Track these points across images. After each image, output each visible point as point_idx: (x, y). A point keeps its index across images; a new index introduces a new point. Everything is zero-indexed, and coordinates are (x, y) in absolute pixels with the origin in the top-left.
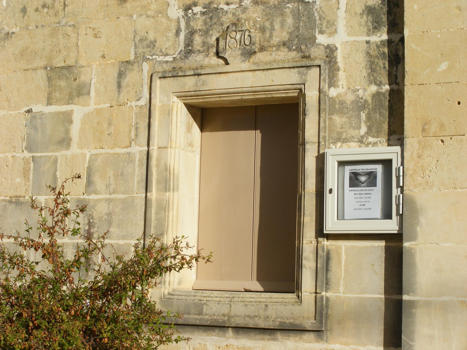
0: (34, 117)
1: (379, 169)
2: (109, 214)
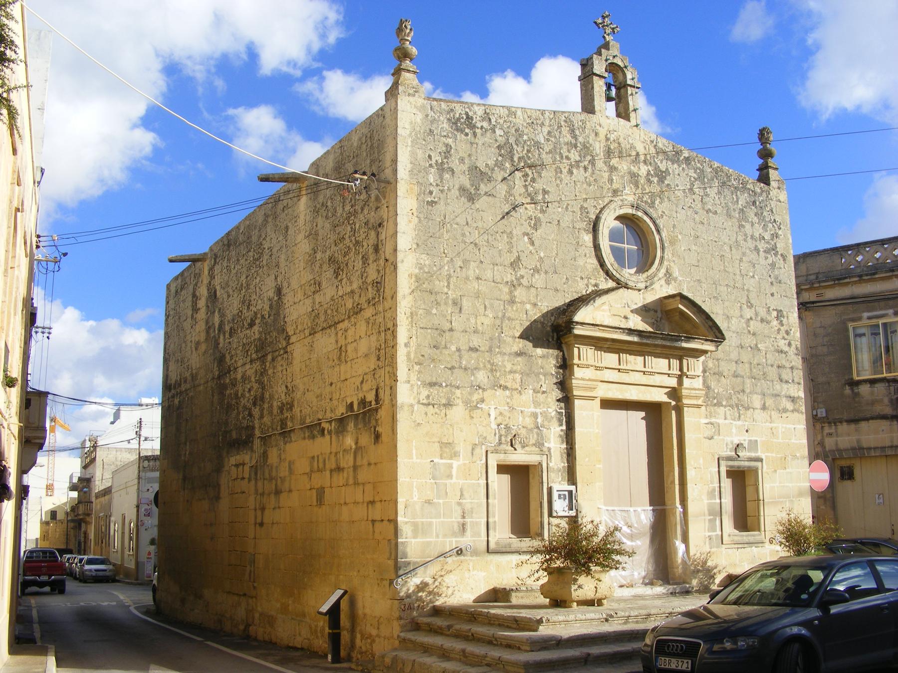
0: (435, 464)
1: (566, 493)
2: (472, 508)
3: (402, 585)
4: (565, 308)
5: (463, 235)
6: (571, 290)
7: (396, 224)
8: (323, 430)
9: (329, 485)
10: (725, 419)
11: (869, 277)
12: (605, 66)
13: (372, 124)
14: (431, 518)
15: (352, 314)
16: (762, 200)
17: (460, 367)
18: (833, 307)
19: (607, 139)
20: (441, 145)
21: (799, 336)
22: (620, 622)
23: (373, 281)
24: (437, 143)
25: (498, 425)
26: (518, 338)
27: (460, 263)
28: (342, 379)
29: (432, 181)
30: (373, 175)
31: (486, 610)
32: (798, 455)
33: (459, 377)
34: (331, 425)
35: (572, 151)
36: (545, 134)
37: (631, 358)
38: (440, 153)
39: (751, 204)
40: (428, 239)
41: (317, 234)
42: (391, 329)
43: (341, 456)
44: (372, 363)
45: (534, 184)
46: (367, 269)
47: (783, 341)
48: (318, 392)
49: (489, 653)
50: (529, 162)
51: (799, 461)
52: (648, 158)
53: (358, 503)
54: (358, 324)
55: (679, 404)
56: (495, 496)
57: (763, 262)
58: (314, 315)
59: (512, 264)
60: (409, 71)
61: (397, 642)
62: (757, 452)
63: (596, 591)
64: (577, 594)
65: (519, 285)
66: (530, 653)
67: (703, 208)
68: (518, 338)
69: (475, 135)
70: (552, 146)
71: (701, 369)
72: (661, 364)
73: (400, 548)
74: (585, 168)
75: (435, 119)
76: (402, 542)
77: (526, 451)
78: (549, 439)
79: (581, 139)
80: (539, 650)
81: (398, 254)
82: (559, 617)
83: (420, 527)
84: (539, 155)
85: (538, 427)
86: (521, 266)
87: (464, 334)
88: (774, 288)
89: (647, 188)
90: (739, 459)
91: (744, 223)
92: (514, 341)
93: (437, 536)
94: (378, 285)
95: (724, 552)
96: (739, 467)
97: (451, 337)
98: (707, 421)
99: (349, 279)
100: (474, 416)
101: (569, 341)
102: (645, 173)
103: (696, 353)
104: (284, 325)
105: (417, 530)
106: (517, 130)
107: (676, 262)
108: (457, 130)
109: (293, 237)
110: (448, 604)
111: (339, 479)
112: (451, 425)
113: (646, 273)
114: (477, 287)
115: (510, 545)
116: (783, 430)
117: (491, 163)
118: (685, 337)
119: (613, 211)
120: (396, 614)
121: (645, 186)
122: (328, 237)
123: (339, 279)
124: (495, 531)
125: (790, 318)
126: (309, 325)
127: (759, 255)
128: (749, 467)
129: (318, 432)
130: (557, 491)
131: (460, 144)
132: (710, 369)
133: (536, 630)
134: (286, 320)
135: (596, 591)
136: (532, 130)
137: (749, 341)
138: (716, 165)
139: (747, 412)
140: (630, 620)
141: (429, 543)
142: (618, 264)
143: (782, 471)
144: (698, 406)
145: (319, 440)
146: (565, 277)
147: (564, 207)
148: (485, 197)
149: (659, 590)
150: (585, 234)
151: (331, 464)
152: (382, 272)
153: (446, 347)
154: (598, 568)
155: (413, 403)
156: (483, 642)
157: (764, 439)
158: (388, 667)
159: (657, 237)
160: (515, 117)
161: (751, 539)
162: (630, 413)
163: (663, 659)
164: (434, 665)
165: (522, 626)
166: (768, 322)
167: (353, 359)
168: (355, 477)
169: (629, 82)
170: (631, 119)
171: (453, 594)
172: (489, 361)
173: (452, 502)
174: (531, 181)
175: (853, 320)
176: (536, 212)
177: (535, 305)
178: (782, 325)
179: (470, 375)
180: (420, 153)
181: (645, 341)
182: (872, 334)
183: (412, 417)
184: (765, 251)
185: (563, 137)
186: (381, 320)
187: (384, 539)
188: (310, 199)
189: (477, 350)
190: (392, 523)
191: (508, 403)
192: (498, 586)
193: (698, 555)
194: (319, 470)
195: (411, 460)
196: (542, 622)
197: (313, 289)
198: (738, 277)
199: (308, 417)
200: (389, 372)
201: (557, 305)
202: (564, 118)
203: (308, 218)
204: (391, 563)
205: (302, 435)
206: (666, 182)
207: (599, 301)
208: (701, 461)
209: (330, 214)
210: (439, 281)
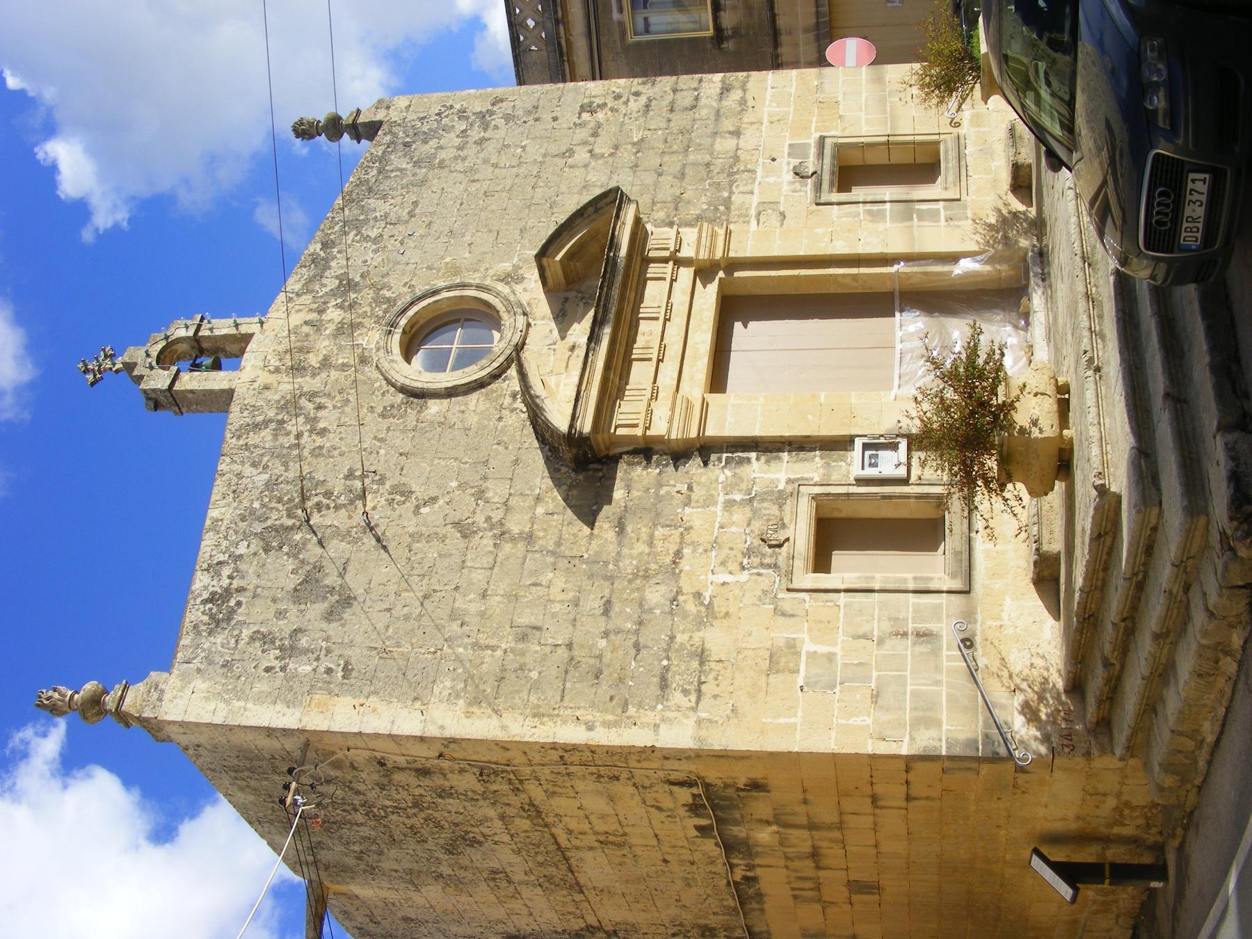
0: (807, 684)
1: (867, 453)
2: (890, 619)
3: (1026, 749)
4: (547, 447)
5: (407, 618)
6: (518, 438)
7: (377, 736)
8: (745, 878)
9: (844, 873)
10: (752, 193)
11: (559, 9)
12: (161, 371)
13: (213, 767)
14: (905, 693)
15: (540, 821)
16: (404, 132)
17: (637, 632)
18: (603, 65)
19: (277, 370)
20: (250, 650)
21: (624, 80)
22: (1100, 346)
23: (479, 781)
24: (246, 656)
25: (743, 568)
26: (592, 529)
27: (455, 626)
28: (655, 842)
29: (309, 668)
30: (290, 771)
31: (1077, 595)
32: (816, 83)
33: (654, 636)
34: (737, 865)
35: (289, 428)
36: (255, 471)
37: (640, 341)
38: (263, 652)
39: (407, 149)
40: (408, 681)
41: (410, 872)
42: (561, 753)
43: (791, 850)
44: (624, 789)
45: (335, 494)
46: (461, 790)
47: (632, 104)
48: (679, 884)
49: (1164, 585)
50: (297, 500)
51: (825, 81)
52: (315, 306)
53: (875, 824)
54: (561, 812)
55: (722, 265)
56: (868, 577)
57: (501, 132)
58: (547, 884)
59: (465, 536)
60: (122, 698)
61: (1132, 762)
62: (809, 145)
63: (1043, 394)
64: (1048, 427)
65: (502, 524)
66: (1165, 506)
67: (407, 222)
68: (592, 529)
69: (241, 590)
70: (277, 461)
71: (666, 229)
72: (654, 293)
73: (958, 751)
74: (320, 407)
75: (206, 658)
76: (948, 748)
77: (791, 520)
78: (772, 481)
79: (271, 414)
80: (1159, 490)
81: (428, 734)
82: (1093, 454)
83: (920, 714)
84: (288, 482)
85: (751, 500)
86: (470, 521)
87: (578, 624)
88: (545, 116)
89: (364, 309)
90: (819, 172)
91: (437, 161)
92: (597, 536)
93: (938, 683)
94: (485, 773)
95: (973, 197)
96: (832, 173)
97: (582, 646)
98: (754, 222)
99: (481, 822)
100: (724, 610)
101: (604, 442)
102: (339, 311)
103: (639, 234)
104: (569, 934)
105: (926, 720)
106: (243, 519)
107: (488, 266)
108: (229, 619)
109: (420, 911)
110: (1061, 666)
111: (833, 854)
112: (738, 652)
113: (501, 313)
114: (498, 598)
115: (957, 554)
116: (775, 105)
117: (290, 564)
118: (610, 250)
119: (395, 365)
120: (1079, 761)
121: (360, 312)
122: (412, 853)
123: (482, 839)
124: (931, 579)
125: (593, 94)
126: (565, 892)
127: (490, 139)
128: (833, 157)
129: (749, 888)
130: (863, 468)
131: (254, 615)
132: (668, 216)
133: (1118, 498)
134: (559, 930)
135: (1043, 394)
136: (246, 493)
137: (626, 154)
138: (339, 201)
139: (742, 159)
140: (1097, 328)
141: (951, 699)
142: (482, 358)
143: (841, 107)
144: (728, 234)
145: (764, 886)
146: (495, 447)
147: (378, 444)
148: (347, 578)
149: (1037, 299)
150: (426, 412)
151: (807, 867)
152: (463, 765)
153: (600, 657)
154: (1001, 390)
155: (695, 719)
156: (1140, 599)
157: (788, 135)
158: (1182, 781)
159: (445, 295)
160: (222, 520)
161: (952, 155)
162: (735, 345)
163: (1184, 234)
164: (1183, 694)
165: (1109, 526)
166: (599, 125)
167: (620, 822)
168: (830, 827)
169: (191, 333)
170: (250, 332)
171: (1043, 657)
172: (630, 581)
173: (876, 656)
174: (329, 499)
175: (623, 34)
176: (381, 491)
177: (538, 499)
178: (605, 105)
179: (651, 616)
180: (259, 687)
181: (612, 316)
182: (645, 7)
183: (720, 722)
184: (485, 130)
185: (264, 442)
186: (547, 770)
187: (941, 780)
188: (352, 878)
189: (609, 602)
190: (913, 765)
191: (706, 551)
192: (1030, 575)
193: (978, 237)
194: (818, 888)
195: (799, 727)
196: (1103, 485)
197: (504, 884)
198: (522, 170)
199: (725, 903)
200: (639, 761)
201: (542, 461)
202: (234, 440)
203: (384, 884)
204: (985, 769)
205: (757, 913)
206: (358, 279)
207: (537, 389)
208: (820, 231)
209: (374, 848)
210: (482, 663)
